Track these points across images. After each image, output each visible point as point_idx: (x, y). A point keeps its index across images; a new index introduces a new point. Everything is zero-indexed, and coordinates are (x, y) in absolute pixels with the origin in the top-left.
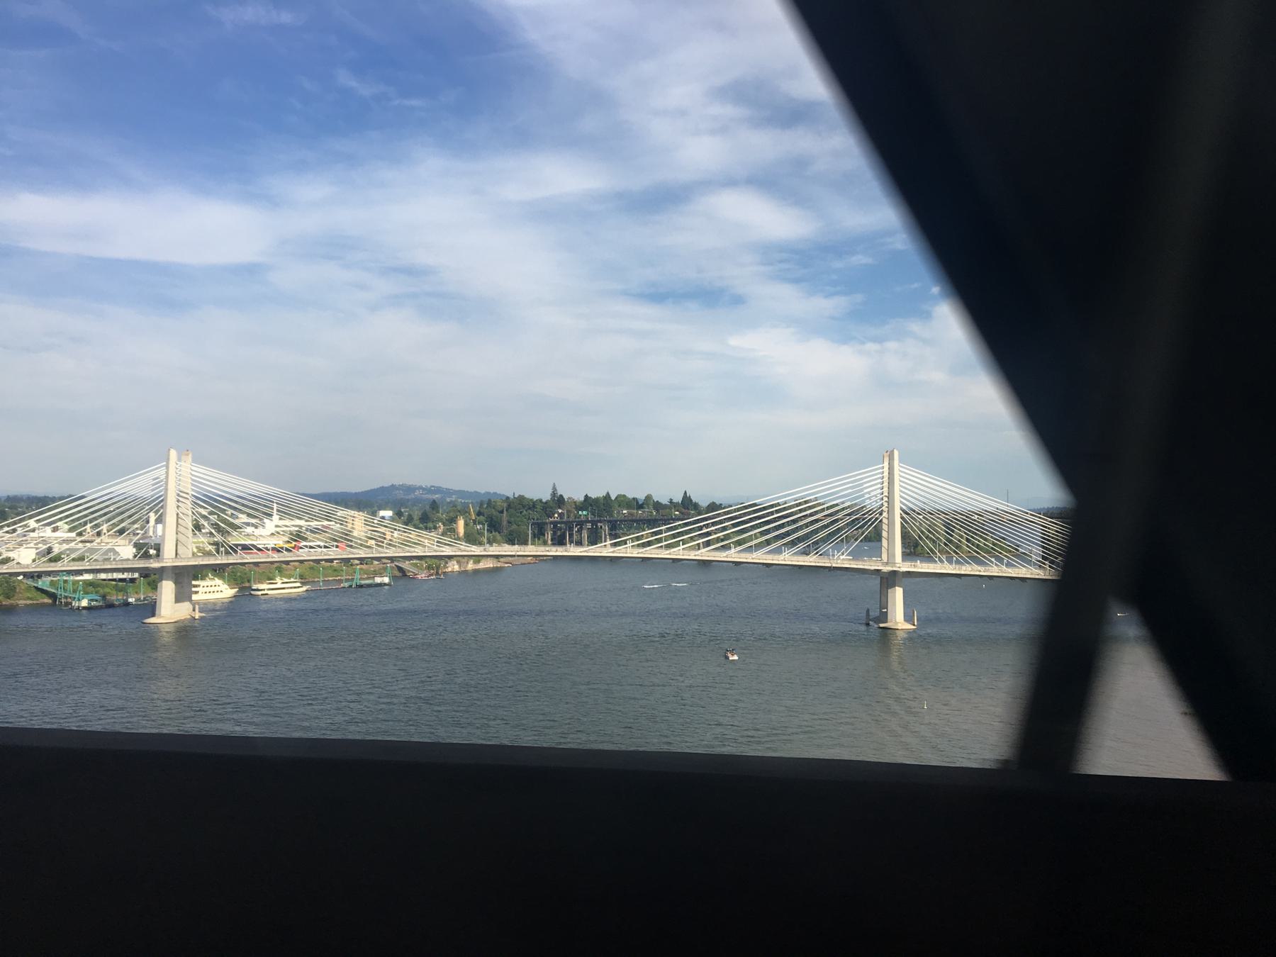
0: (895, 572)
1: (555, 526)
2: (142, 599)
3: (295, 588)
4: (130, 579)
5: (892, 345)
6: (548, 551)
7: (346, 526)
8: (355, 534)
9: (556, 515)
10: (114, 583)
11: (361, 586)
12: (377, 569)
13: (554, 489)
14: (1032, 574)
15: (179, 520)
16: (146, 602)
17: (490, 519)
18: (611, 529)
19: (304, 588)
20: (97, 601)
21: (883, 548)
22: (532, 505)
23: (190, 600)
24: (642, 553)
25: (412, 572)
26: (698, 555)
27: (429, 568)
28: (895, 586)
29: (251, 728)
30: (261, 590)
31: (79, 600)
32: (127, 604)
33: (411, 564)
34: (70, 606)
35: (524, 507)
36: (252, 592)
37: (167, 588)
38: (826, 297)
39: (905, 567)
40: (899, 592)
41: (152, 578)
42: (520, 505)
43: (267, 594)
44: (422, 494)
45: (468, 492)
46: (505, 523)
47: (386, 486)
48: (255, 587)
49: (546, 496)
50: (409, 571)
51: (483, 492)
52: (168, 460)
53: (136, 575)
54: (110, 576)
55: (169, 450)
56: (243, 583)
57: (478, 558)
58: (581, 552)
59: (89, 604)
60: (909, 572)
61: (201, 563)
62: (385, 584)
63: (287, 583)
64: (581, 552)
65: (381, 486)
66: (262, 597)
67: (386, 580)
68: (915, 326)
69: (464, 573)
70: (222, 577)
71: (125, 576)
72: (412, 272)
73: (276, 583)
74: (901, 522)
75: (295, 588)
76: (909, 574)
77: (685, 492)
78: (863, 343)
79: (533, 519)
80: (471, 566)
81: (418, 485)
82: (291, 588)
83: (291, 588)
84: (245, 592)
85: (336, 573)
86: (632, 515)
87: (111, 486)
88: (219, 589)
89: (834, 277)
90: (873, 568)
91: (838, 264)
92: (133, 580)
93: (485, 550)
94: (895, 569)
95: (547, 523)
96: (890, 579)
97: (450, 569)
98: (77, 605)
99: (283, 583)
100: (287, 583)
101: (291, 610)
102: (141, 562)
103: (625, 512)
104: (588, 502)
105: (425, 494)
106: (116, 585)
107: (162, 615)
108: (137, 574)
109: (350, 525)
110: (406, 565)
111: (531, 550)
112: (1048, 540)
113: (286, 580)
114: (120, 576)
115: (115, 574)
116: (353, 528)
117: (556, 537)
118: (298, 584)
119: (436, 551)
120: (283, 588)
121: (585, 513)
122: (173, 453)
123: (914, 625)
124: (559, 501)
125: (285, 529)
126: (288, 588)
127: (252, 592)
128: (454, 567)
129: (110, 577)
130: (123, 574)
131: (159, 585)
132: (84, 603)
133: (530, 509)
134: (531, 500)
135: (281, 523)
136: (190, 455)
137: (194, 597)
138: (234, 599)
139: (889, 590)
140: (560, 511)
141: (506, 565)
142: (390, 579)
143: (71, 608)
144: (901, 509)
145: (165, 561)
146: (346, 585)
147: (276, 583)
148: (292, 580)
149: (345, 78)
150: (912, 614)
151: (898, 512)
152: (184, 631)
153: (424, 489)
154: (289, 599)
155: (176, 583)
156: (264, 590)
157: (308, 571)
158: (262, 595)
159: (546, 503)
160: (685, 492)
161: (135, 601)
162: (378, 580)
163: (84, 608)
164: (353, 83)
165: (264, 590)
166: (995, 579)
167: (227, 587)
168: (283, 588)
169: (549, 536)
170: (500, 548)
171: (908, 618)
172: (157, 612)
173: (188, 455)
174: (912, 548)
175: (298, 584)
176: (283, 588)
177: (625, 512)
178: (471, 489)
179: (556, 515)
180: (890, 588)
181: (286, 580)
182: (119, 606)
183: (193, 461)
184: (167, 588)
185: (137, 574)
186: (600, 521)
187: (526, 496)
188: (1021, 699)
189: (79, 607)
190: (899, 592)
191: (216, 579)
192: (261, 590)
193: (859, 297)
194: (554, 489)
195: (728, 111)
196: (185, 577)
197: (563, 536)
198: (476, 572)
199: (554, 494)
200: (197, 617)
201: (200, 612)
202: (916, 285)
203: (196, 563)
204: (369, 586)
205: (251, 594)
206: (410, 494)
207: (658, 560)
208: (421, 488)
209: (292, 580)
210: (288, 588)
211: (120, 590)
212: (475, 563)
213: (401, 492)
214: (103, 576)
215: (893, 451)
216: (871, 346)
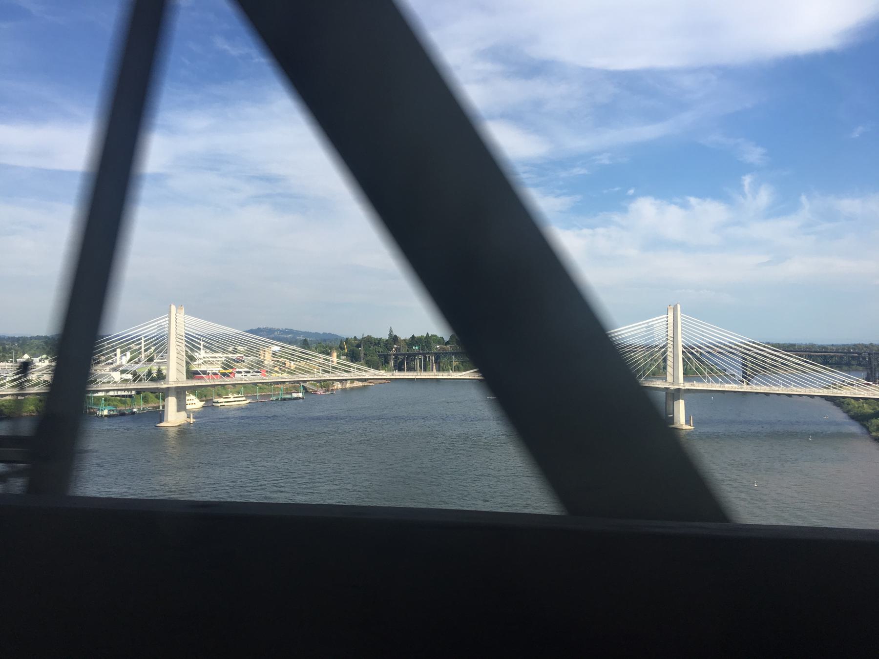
0: (678, 390)
1: (396, 357)
2: (142, 409)
3: (242, 401)
4: (129, 395)
5: (601, 230)
6: (437, 375)
7: (260, 358)
8: (266, 362)
9: (394, 349)
10: (118, 398)
11: (284, 399)
12: (288, 387)
13: (391, 331)
14: (773, 390)
15: (672, 373)
16: (145, 411)
17: (351, 353)
18: (435, 359)
19: (248, 401)
20: (113, 411)
21: (668, 373)
22: (378, 342)
23: (185, 410)
24: (462, 375)
25: (312, 389)
26: (462, 375)
27: (321, 387)
28: (679, 399)
29: (118, 495)
30: (221, 402)
31: (102, 410)
32: (134, 413)
33: (310, 384)
34: (95, 415)
35: (371, 343)
36: (214, 404)
37: (172, 402)
38: (556, 197)
39: (688, 386)
40: (682, 403)
41: (164, 394)
42: (369, 342)
43: (224, 405)
44: (279, 334)
45: (311, 333)
46: (362, 355)
47: (255, 329)
48: (215, 400)
49: (385, 336)
50: (310, 389)
51: (321, 333)
52: (170, 313)
53: (133, 393)
54: (115, 393)
55: (171, 305)
56: (202, 397)
57: (352, 380)
58: (460, 376)
59: (108, 412)
60: (689, 389)
61: (197, 384)
62: (300, 398)
63: (237, 397)
64: (460, 376)
65: (251, 329)
66: (222, 407)
67: (300, 395)
68: (616, 217)
69: (344, 390)
70: (194, 394)
71: (126, 393)
72: (269, 179)
73: (230, 398)
74: (683, 358)
75: (242, 401)
76: (688, 391)
77: (391, 328)
78: (581, 229)
79: (379, 352)
80: (348, 385)
81: (277, 328)
82: (240, 401)
83: (240, 401)
84: (210, 406)
85: (261, 391)
86: (444, 349)
87: (135, 329)
88: (193, 402)
89: (561, 183)
90: (663, 387)
91: (563, 174)
92: (130, 396)
93: (752, 389)
94: (678, 387)
95: (390, 355)
96: (676, 394)
97: (335, 387)
98: (100, 414)
99: (234, 397)
100: (237, 397)
101: (244, 417)
102: (150, 384)
103: (438, 347)
104: (414, 341)
105: (282, 334)
106: (121, 399)
107: (169, 421)
108: (134, 392)
109: (262, 357)
110: (307, 385)
111: (383, 374)
112: (128, 340)
113: (236, 396)
114: (123, 393)
115: (119, 392)
116: (264, 360)
117: (397, 364)
118: (244, 398)
119: (358, 375)
120: (233, 401)
121: (417, 348)
122: (173, 308)
123: (691, 426)
124: (394, 339)
125: (219, 359)
126: (238, 401)
127: (214, 404)
128: (338, 386)
129: (116, 394)
130: (125, 392)
131: (166, 400)
132: (106, 412)
133: (376, 344)
134: (377, 339)
135: (206, 355)
136: (183, 310)
137: (188, 407)
138: (202, 409)
139: (675, 402)
140: (395, 346)
141: (371, 384)
142: (303, 394)
143: (96, 416)
144: (683, 346)
145: (170, 383)
146: (274, 398)
147: (230, 398)
148: (240, 395)
149: (221, 43)
150: (689, 419)
151: (680, 349)
152: (183, 431)
153: (281, 331)
154: (240, 409)
155: (177, 398)
156: (222, 402)
157: (246, 388)
158: (221, 406)
159: (387, 341)
160: (391, 328)
161: (138, 411)
162: (295, 395)
163: (106, 416)
164: (226, 47)
165: (222, 402)
166: (815, 397)
167: (198, 401)
168: (235, 401)
169: (392, 363)
170: (377, 372)
171: (688, 422)
172: (165, 419)
173: (182, 309)
174: (688, 374)
175: (244, 398)
176: (235, 401)
177: (438, 347)
178: (313, 331)
179: (394, 349)
180: (676, 400)
181: (236, 396)
182: (128, 414)
183: (185, 313)
184: (172, 402)
185: (134, 392)
186: (428, 353)
187: (373, 336)
188: (87, 451)
189: (102, 415)
190: (682, 403)
191: (191, 395)
192: (221, 402)
193: (578, 197)
194: (391, 331)
195: (488, 67)
196: (180, 393)
197: (402, 363)
198: (352, 389)
199: (391, 335)
200: (192, 422)
201: (193, 419)
202: (617, 189)
203: (193, 385)
204: (290, 399)
205: (213, 406)
206: (271, 335)
207: (461, 380)
208: (278, 330)
209: (240, 395)
210: (238, 401)
211: (124, 403)
212: (351, 383)
213: (265, 333)
214: (111, 393)
215: (676, 305)
216: (586, 231)
